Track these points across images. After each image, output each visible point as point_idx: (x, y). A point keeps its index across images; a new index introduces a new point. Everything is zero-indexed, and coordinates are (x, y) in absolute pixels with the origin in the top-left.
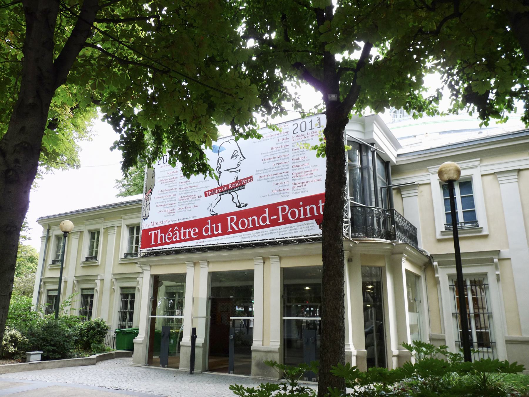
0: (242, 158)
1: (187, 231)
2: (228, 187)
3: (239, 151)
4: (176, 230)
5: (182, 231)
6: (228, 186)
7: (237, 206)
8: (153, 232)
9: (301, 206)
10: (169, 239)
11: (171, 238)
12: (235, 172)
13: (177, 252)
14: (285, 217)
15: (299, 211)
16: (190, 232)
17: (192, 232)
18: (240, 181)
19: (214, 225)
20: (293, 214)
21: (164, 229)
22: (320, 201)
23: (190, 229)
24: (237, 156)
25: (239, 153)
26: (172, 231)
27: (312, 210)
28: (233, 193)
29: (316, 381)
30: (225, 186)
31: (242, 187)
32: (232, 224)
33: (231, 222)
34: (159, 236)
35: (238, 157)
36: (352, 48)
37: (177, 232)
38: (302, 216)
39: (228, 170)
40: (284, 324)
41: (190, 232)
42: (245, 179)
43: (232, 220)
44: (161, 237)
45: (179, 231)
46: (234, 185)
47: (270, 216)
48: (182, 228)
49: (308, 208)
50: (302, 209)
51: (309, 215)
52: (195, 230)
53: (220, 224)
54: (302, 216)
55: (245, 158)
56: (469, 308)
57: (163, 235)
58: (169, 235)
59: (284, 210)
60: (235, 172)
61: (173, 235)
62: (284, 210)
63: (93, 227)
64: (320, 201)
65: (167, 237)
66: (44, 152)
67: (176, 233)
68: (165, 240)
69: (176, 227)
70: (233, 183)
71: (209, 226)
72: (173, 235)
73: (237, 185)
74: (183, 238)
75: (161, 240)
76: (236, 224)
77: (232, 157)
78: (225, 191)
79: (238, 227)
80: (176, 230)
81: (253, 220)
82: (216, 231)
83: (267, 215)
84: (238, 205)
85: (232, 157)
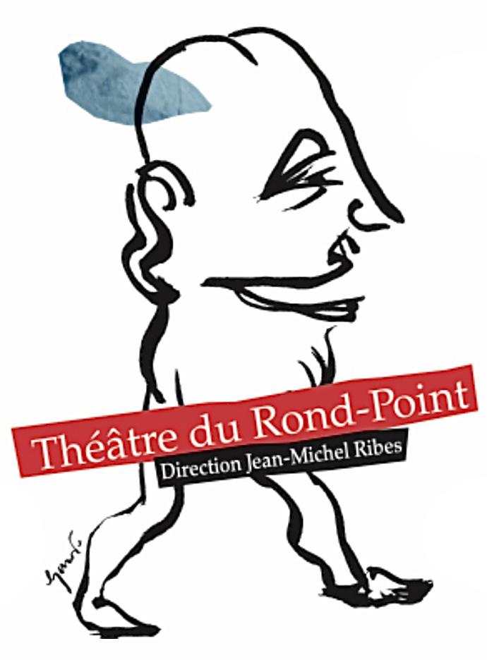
0: (370, 213)
1: (147, 437)
2: (248, 426)
3: (335, 139)
4: (114, 435)
5: (132, 438)
6: (240, 410)
7: (332, 589)
9: (419, 392)
11: (105, 453)
12: (309, 311)
15: (417, 401)
17: (161, 441)
18: (359, 388)
19: (220, 426)
20: (404, 406)
22: (459, 385)
23: (154, 435)
24: (320, 183)
25: (341, 163)
27: (442, 398)
28: (296, 484)
30: (220, 411)
31: (376, 447)
32: (267, 422)
33: (263, 418)
34: (65, 450)
35: (336, 199)
37: (119, 440)
38: (424, 411)
39: (238, 286)
42: (404, 384)
43: (265, 414)
45: (125, 437)
46: (307, 422)
48: (131, 432)
49: (434, 395)
50: (421, 397)
51: (437, 410)
53: (234, 424)
54: (424, 411)
55: (397, 216)
58: (95, 446)
59: (384, 397)
60: (309, 311)
61: (107, 448)
62: (384, 397)
64: (459, 385)
65: (88, 452)
68: (85, 458)
70: (285, 402)
71: (207, 427)
73: (331, 422)
74: (135, 454)
76: (277, 423)
77: (278, 183)
78: (224, 454)
79: (280, 429)
80: (114, 435)
81: (317, 417)
82: (227, 438)
83: (347, 407)
84: (344, 577)
85: (278, 183)
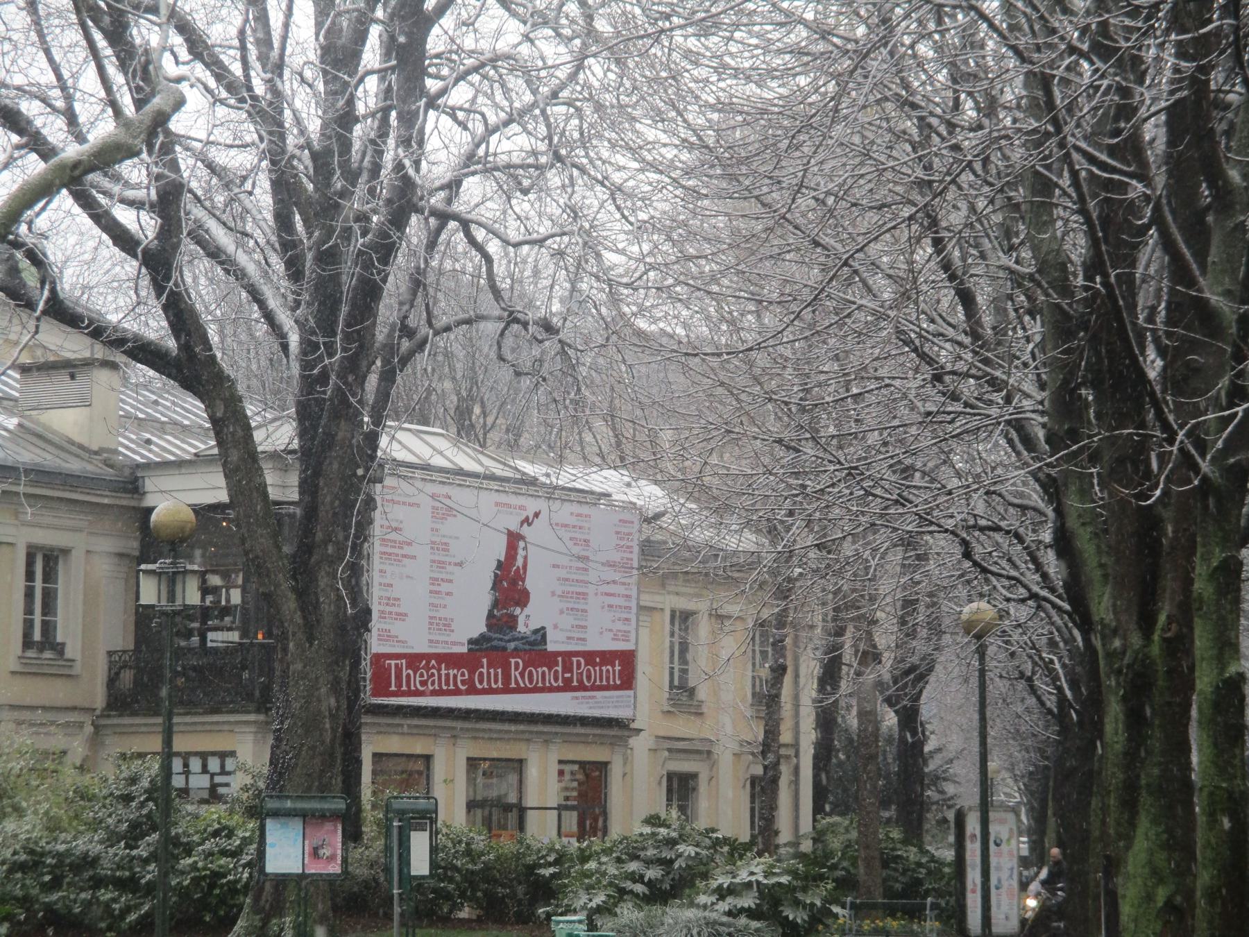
4: (433, 667)
5: (443, 672)
8: (393, 662)
10: (423, 683)
13: (435, 713)
14: (580, 681)
16: (455, 677)
17: (459, 678)
21: (414, 660)
26: (427, 668)
29: (434, 865)
36: (1045, 233)
40: (124, 733)
41: (455, 677)
44: (408, 676)
45: (439, 670)
47: (563, 672)
52: (463, 675)
56: (120, 716)
57: (410, 672)
58: (422, 675)
61: (429, 677)
63: (683, 604)
65: (418, 679)
66: (180, 145)
67: (433, 675)
68: (455, 684)
69: (433, 662)
71: (485, 671)
72: (429, 677)
75: (399, 685)
80: (433, 667)
83: (559, 669)
